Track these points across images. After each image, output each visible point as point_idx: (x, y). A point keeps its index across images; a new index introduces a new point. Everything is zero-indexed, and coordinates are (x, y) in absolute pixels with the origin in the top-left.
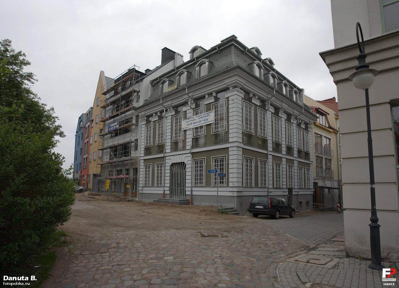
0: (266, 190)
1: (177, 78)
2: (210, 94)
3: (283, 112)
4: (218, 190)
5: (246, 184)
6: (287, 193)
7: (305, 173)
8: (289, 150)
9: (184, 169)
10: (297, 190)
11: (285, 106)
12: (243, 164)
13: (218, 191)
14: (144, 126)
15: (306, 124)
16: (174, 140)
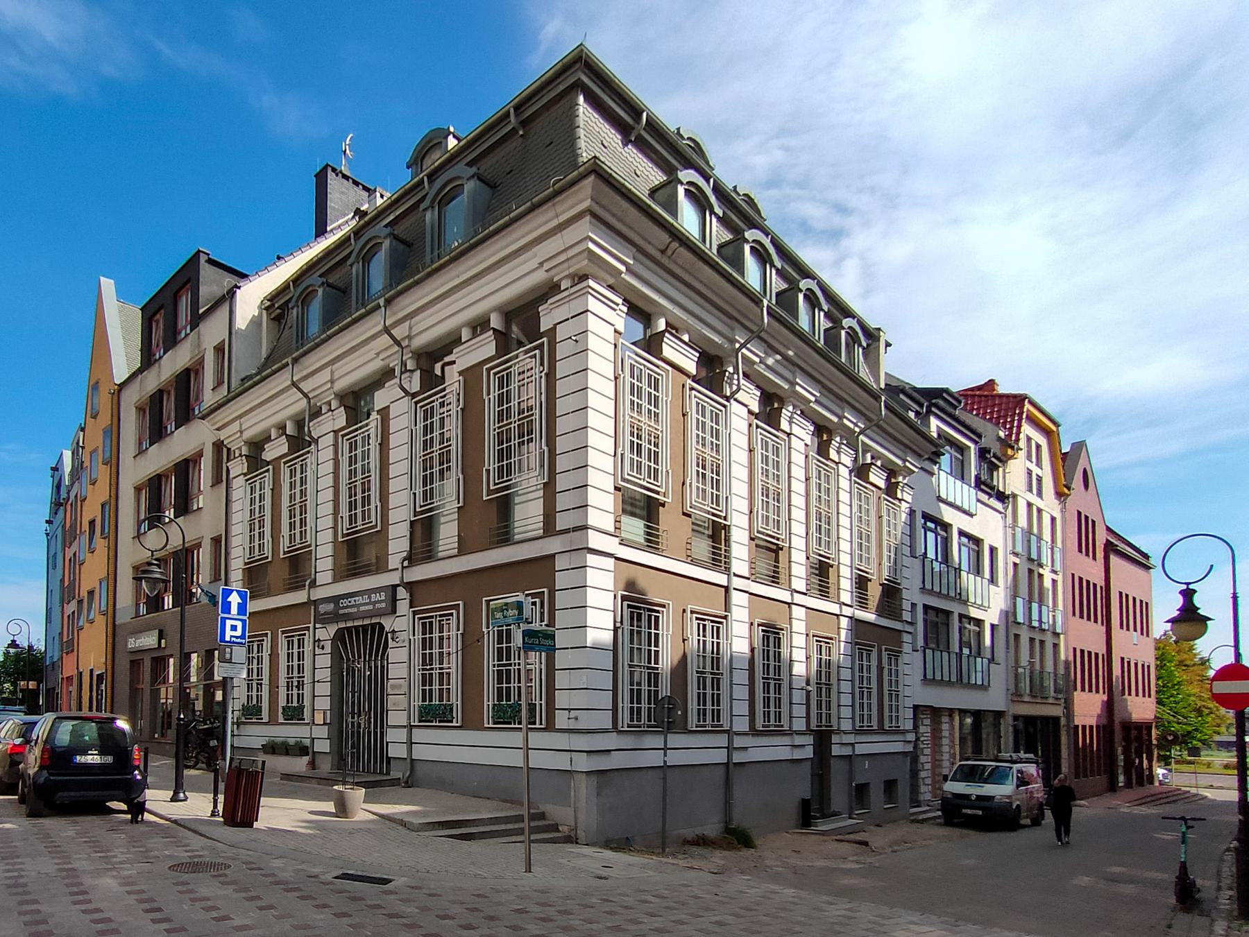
0: (722, 740)
1: (428, 215)
2: (479, 326)
3: (799, 412)
5: (632, 720)
6: (808, 753)
7: (880, 669)
8: (822, 571)
10: (850, 739)
11: (806, 390)
12: (620, 631)
13: (665, 749)
14: (242, 479)
15: (891, 472)
16: (286, 550)
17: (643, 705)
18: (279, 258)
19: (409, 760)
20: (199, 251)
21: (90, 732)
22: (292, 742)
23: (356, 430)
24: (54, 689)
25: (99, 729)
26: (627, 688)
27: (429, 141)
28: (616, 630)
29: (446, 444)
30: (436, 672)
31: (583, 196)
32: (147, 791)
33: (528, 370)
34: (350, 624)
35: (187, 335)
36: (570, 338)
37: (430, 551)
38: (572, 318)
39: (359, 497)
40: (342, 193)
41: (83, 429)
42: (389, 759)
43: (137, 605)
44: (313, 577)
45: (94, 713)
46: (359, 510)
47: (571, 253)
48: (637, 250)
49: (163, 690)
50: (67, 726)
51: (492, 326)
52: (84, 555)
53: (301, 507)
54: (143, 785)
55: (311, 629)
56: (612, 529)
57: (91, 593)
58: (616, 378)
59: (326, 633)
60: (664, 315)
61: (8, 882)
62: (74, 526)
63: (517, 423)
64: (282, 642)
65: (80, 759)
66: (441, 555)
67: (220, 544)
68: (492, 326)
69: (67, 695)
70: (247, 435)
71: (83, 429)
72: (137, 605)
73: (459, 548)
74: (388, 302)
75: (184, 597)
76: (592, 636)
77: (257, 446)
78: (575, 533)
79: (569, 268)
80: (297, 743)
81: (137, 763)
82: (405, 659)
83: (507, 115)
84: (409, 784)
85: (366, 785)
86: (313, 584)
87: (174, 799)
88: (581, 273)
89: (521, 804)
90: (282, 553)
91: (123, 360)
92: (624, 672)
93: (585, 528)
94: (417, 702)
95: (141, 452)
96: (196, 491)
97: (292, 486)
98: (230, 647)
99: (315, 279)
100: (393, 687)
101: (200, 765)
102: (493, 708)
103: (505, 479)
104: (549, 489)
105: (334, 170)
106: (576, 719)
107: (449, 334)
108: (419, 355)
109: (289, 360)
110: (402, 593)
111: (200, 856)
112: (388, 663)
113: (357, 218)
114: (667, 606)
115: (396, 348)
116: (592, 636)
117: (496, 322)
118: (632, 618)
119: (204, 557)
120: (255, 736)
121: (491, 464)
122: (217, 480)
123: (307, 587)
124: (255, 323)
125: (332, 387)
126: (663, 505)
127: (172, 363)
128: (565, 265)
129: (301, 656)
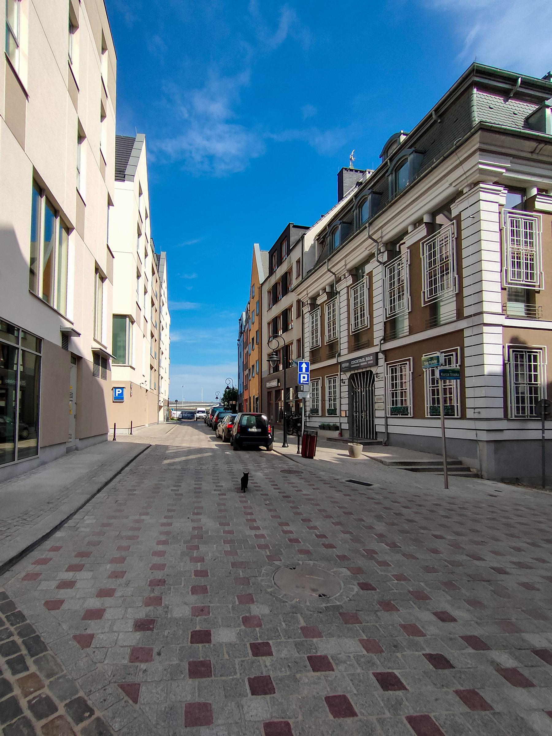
1: (390, 178)
2: (418, 223)
4: (543, 426)
9: (372, 384)
12: (508, 366)
13: (543, 430)
16: (353, 331)
17: (526, 405)
18: (322, 216)
19: (386, 433)
20: (290, 224)
21: (253, 420)
22: (332, 424)
23: (357, 284)
24: (241, 404)
25: (256, 419)
26: (514, 395)
27: (391, 141)
28: (504, 365)
29: (401, 283)
30: (399, 392)
31: (475, 143)
32: (273, 443)
33: (445, 238)
34: (356, 372)
35: (285, 259)
36: (469, 217)
37: (435, 321)
38: (470, 206)
39: (359, 314)
40: (350, 178)
41: (249, 303)
42: (376, 432)
43: (270, 369)
44: (339, 352)
45: (255, 413)
46: (359, 320)
47: (468, 174)
48: (513, 158)
49: (280, 403)
50: (246, 417)
51: (424, 221)
52: (251, 351)
53: (333, 322)
54: (272, 440)
55: (339, 375)
56: (500, 311)
57: (253, 366)
58: (501, 230)
59: (346, 376)
60: (535, 186)
61: (228, 471)
62: (247, 340)
63: (440, 266)
64: (327, 381)
65: (250, 430)
66: (401, 336)
67: (300, 342)
68: (424, 221)
69: (246, 405)
70: (310, 295)
71: (249, 303)
72: (270, 369)
73: (409, 333)
74: (370, 224)
75: (287, 365)
76: (487, 370)
77: (314, 299)
78: (475, 317)
79: (467, 182)
80: (334, 425)
81: (269, 432)
82: (383, 386)
83: (431, 115)
84: (386, 444)
85: (364, 444)
86: (339, 355)
87: (284, 446)
88: (475, 182)
89: (441, 455)
90: (325, 343)
91: (262, 273)
92: (511, 386)
93: (481, 313)
94: (389, 406)
95: (270, 309)
96: (290, 321)
97: (329, 313)
98: (303, 385)
99: (337, 222)
100: (378, 399)
101: (294, 434)
102: (430, 408)
103: (434, 295)
104: (459, 296)
105: (346, 169)
106: (479, 413)
107: (403, 230)
108: (386, 244)
109: (326, 260)
110: (381, 356)
111: (292, 468)
112: (375, 388)
113: (357, 187)
114: (543, 349)
115: (375, 244)
116: (487, 370)
117: (426, 219)
118: (516, 357)
119: (294, 348)
120: (316, 422)
121: (425, 288)
122: (298, 316)
123: (336, 357)
124: (313, 247)
125: (345, 268)
126: (538, 292)
127: (280, 271)
128: (465, 181)
129: (334, 387)
